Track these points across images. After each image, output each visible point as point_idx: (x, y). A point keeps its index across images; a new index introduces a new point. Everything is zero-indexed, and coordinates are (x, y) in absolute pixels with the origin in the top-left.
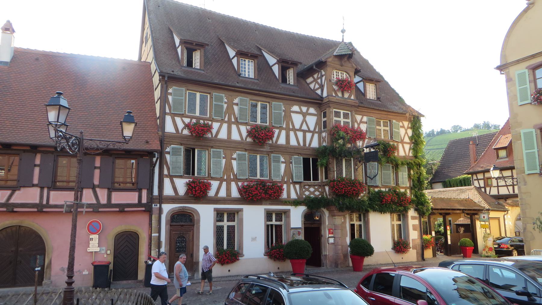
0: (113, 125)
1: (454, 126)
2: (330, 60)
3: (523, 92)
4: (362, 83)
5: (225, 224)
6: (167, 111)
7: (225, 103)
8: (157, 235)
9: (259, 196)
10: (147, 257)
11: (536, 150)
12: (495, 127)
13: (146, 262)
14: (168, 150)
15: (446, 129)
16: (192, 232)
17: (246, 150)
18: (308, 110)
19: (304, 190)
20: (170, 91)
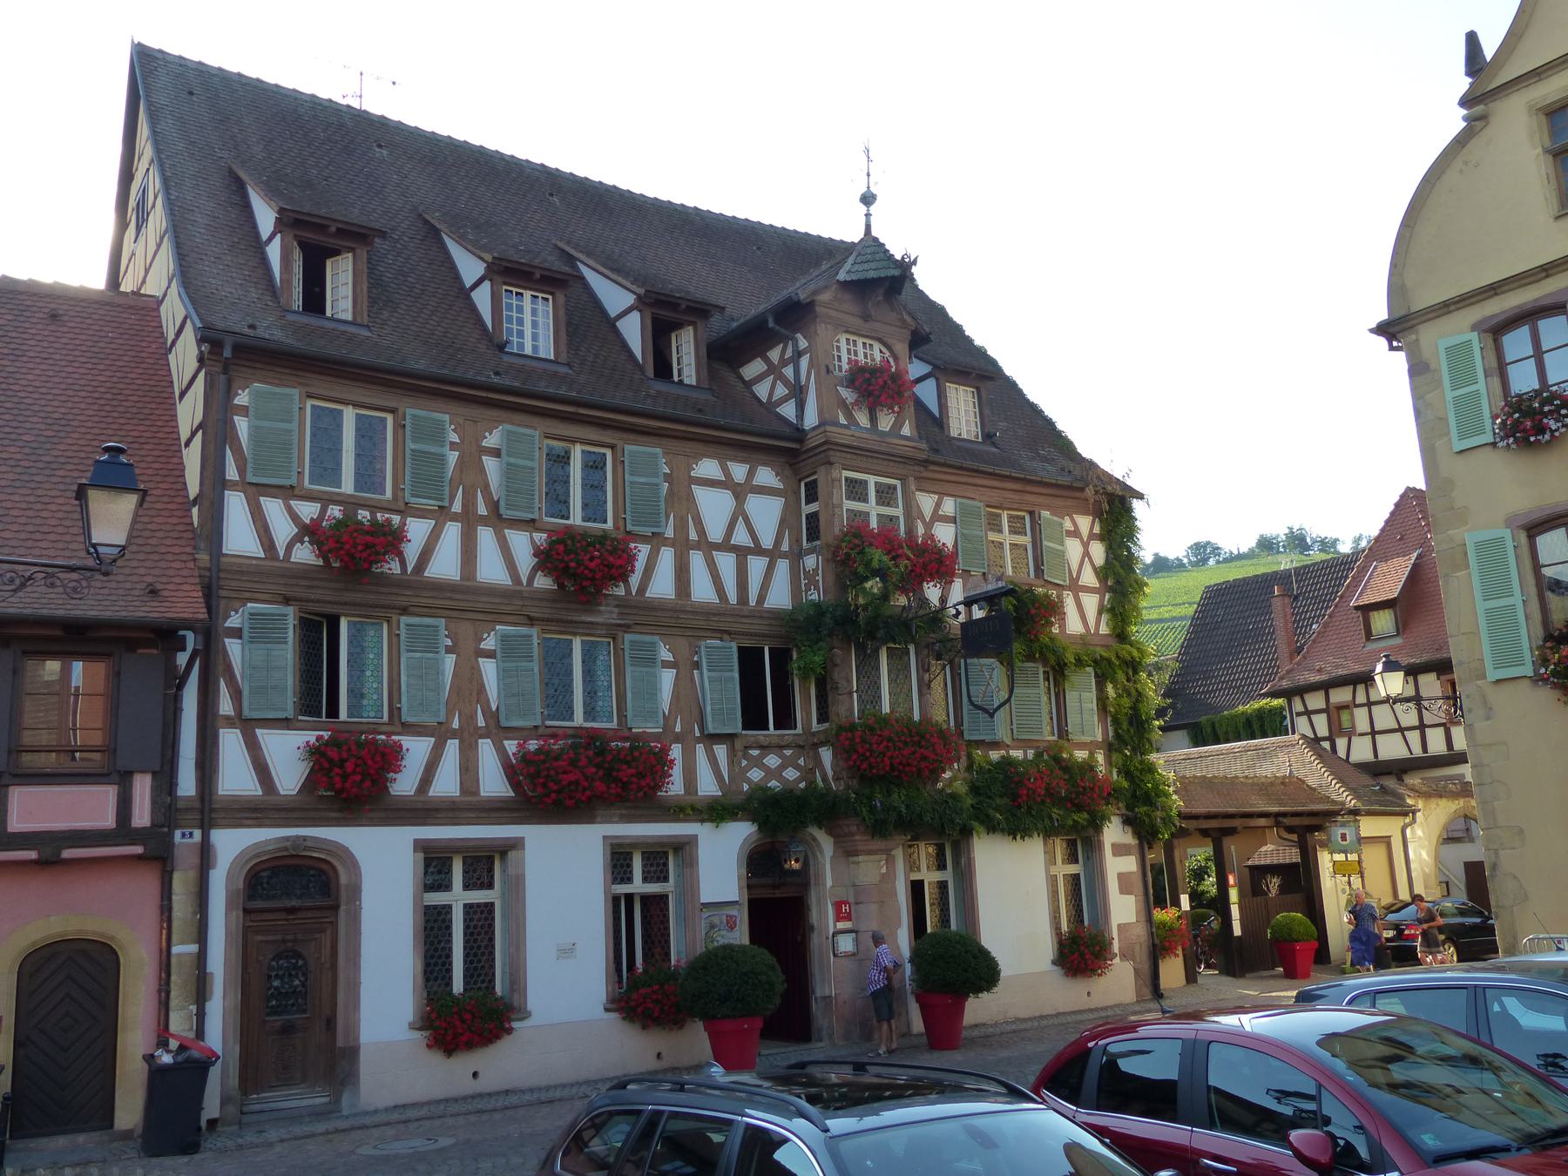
0: (15, 527)
1: (1195, 544)
2: (825, 297)
3: (1465, 407)
4: (931, 383)
5: (458, 897)
6: (232, 473)
7: (453, 446)
8: (193, 948)
9: (584, 789)
10: (153, 1039)
11: (1517, 599)
12: (1326, 545)
13: (149, 1059)
14: (234, 621)
15: (1172, 556)
16: (328, 932)
17: (531, 621)
18: (751, 474)
19: (744, 763)
20: (242, 399)
